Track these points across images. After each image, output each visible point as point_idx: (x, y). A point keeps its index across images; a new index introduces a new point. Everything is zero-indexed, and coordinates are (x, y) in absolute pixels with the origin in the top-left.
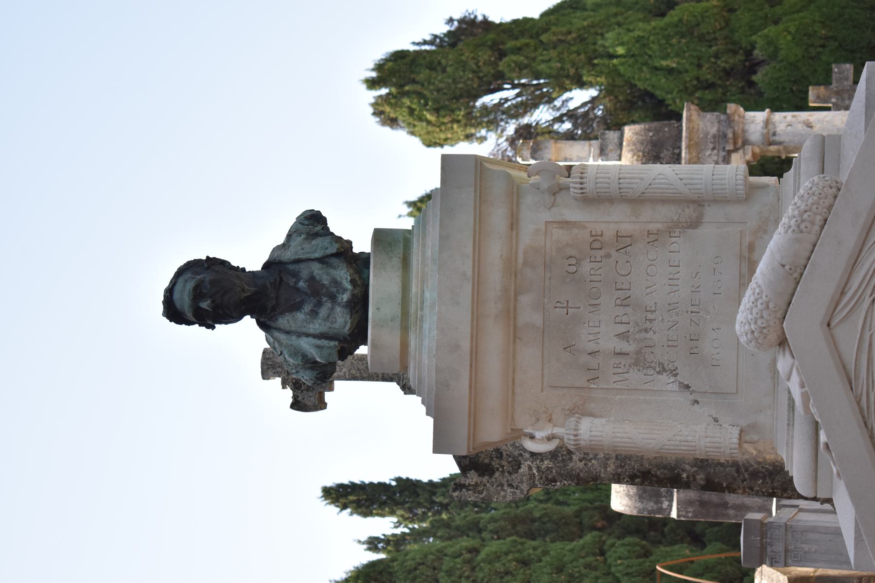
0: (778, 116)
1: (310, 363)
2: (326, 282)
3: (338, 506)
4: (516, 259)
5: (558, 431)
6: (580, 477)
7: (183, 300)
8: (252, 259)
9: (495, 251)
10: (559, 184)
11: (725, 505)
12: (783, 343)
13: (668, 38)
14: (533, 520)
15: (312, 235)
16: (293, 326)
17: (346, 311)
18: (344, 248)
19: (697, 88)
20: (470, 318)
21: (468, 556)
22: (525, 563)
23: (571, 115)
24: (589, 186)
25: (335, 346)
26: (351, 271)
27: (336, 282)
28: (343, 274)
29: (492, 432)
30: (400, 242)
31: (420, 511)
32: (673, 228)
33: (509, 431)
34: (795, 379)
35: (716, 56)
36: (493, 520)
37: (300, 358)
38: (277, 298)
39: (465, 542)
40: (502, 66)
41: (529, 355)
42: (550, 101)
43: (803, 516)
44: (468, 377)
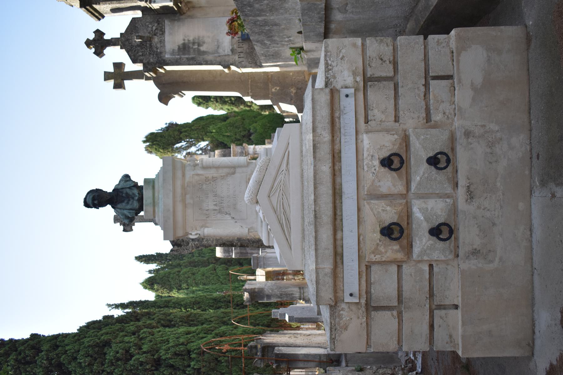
0: (257, 147)
1: (127, 217)
5: (199, 232)
6: (205, 246)
7: (89, 201)
8: (109, 188)
11: (247, 253)
12: (257, 202)
13: (227, 127)
14: (195, 262)
18: (136, 185)
19: (235, 141)
21: (177, 273)
22: (194, 274)
23: (201, 149)
24: (204, 164)
27: (134, 194)
28: (136, 192)
29: (180, 234)
31: (163, 262)
32: (228, 174)
34: (261, 212)
35: (240, 132)
36: (184, 263)
39: (176, 269)
40: (181, 136)
42: (195, 145)
43: (268, 254)
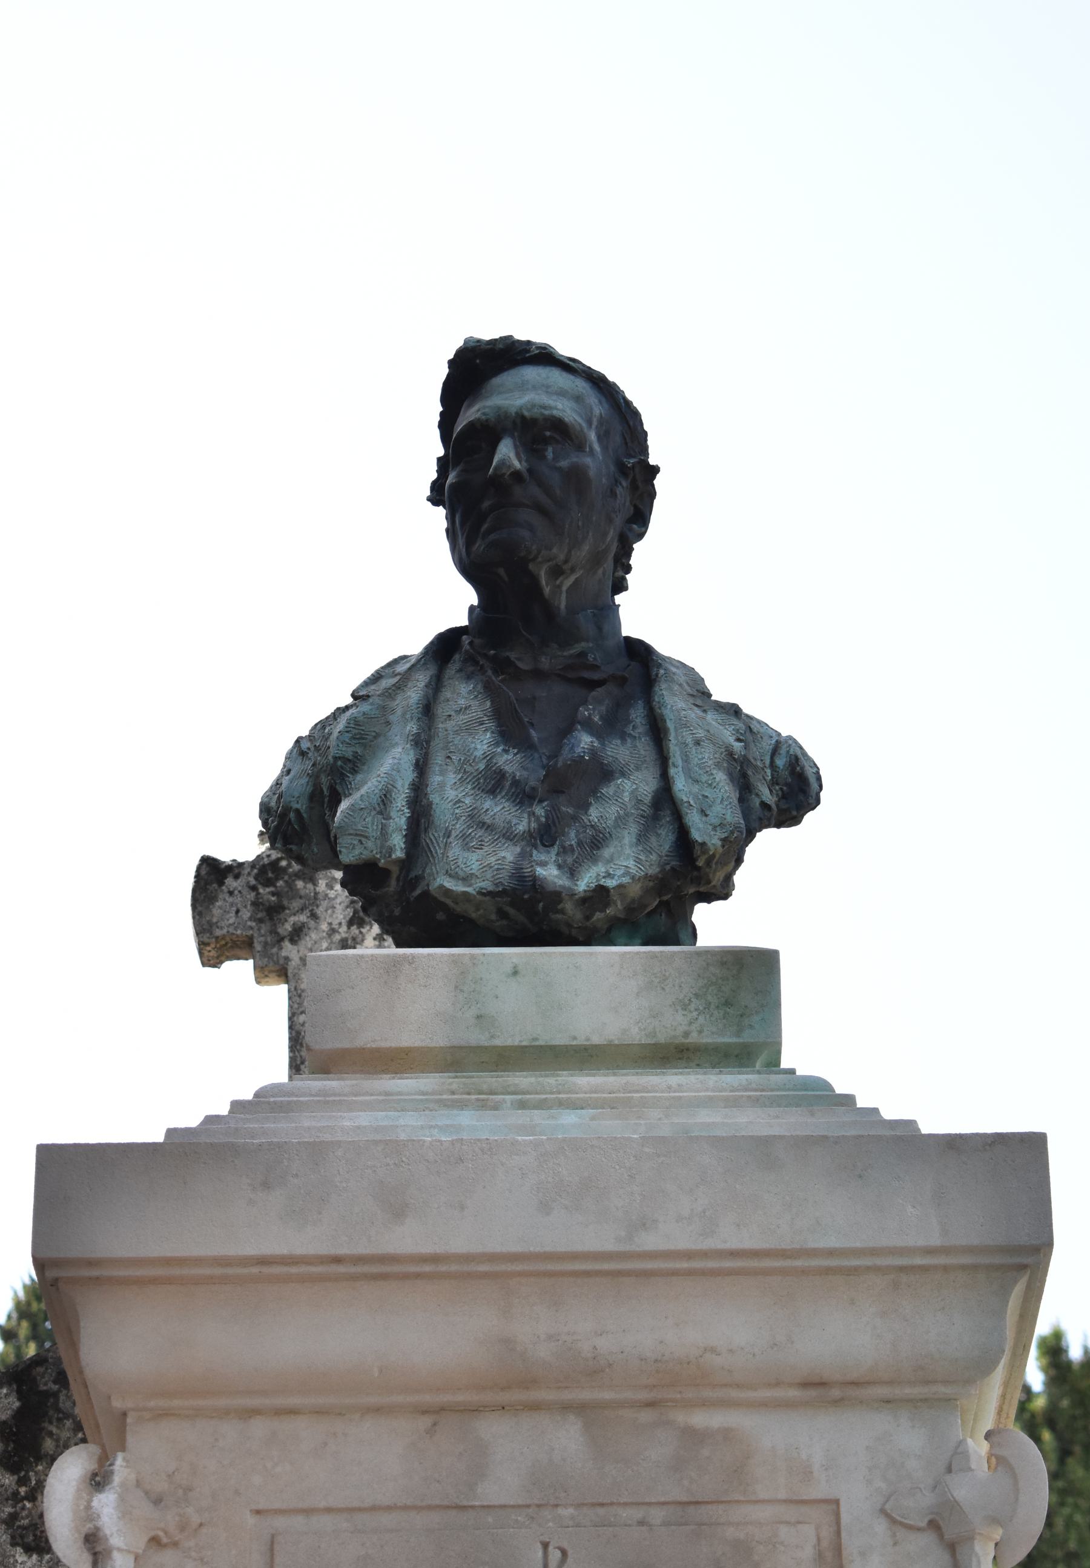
2: (594, 814)
3: (9, 1317)
4: (705, 1404)
7: (515, 393)
9: (729, 1329)
10: (971, 1539)
15: (744, 775)
16: (450, 725)
17: (504, 876)
20: (498, 1249)
25: (391, 850)
26: (635, 891)
27: (595, 843)
28: (624, 864)
30: (738, 1034)
33: (117, 1404)
37: (349, 753)
38: (538, 674)
41: (378, 1460)
44: (300, 1250)
